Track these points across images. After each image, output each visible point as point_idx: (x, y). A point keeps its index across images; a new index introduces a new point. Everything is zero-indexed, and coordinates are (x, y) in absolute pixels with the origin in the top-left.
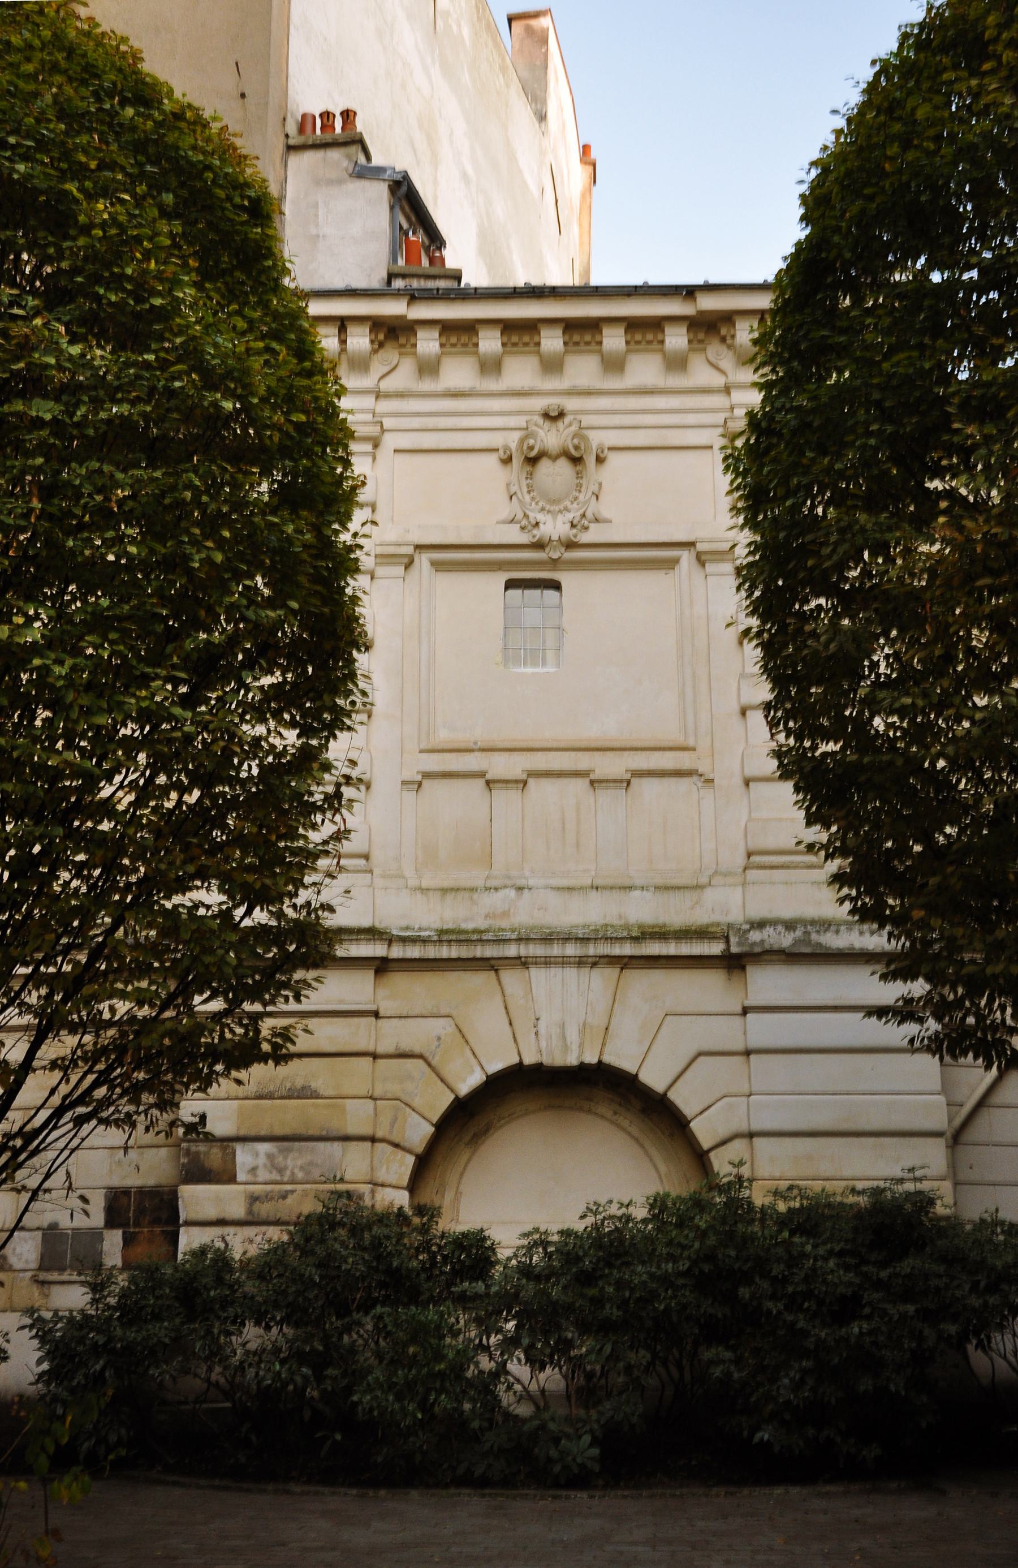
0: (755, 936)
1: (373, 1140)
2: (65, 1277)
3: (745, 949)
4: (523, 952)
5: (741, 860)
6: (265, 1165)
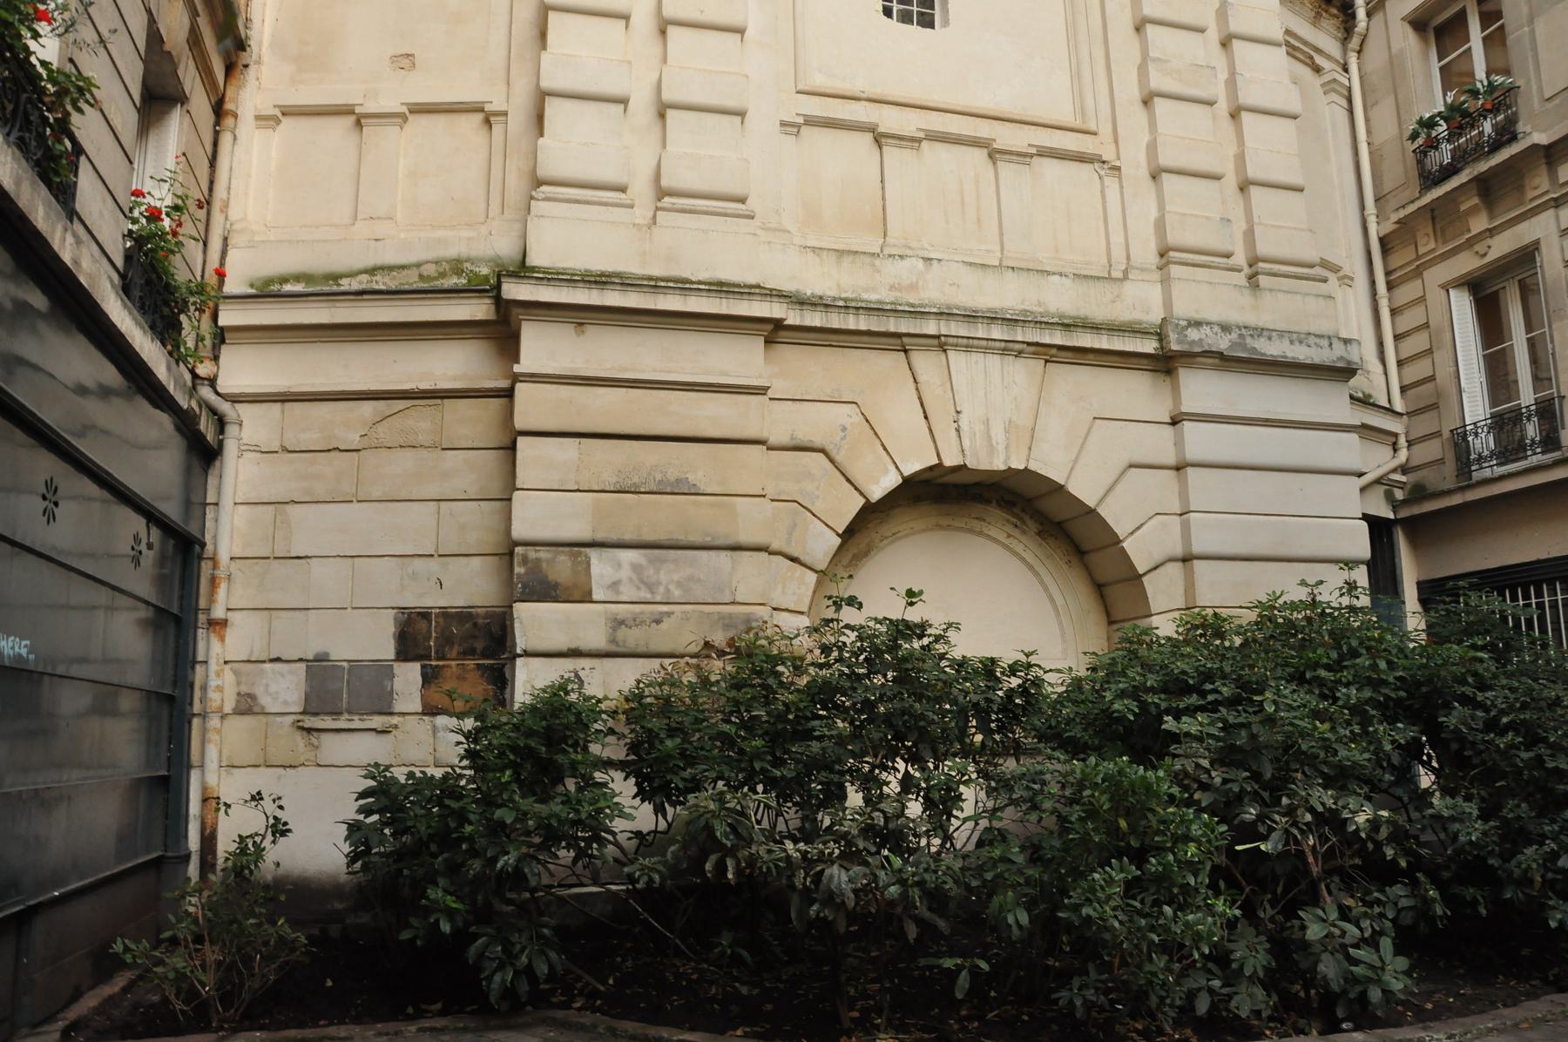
0: (1193, 334)
2: (342, 724)
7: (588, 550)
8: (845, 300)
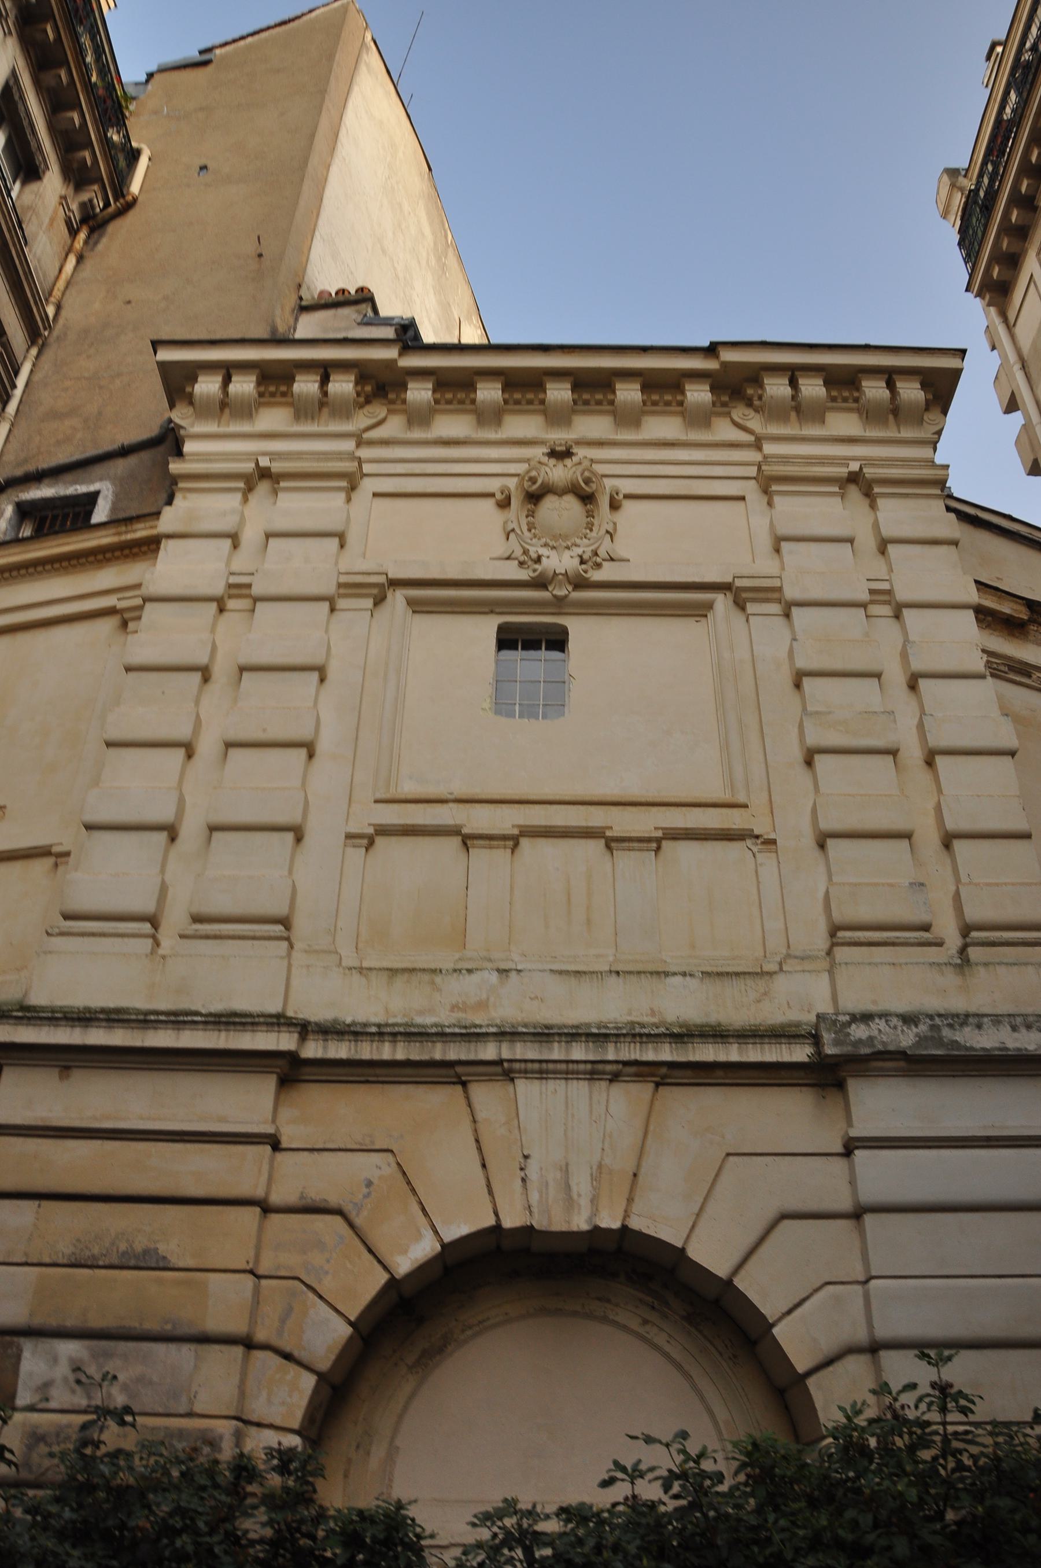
0: (859, 1032)
1: (249, 1344)
3: (847, 1049)
4: (506, 1054)
5: (821, 942)
6: (65, 1379)
7: (22, 1340)
8: (379, 1026)
